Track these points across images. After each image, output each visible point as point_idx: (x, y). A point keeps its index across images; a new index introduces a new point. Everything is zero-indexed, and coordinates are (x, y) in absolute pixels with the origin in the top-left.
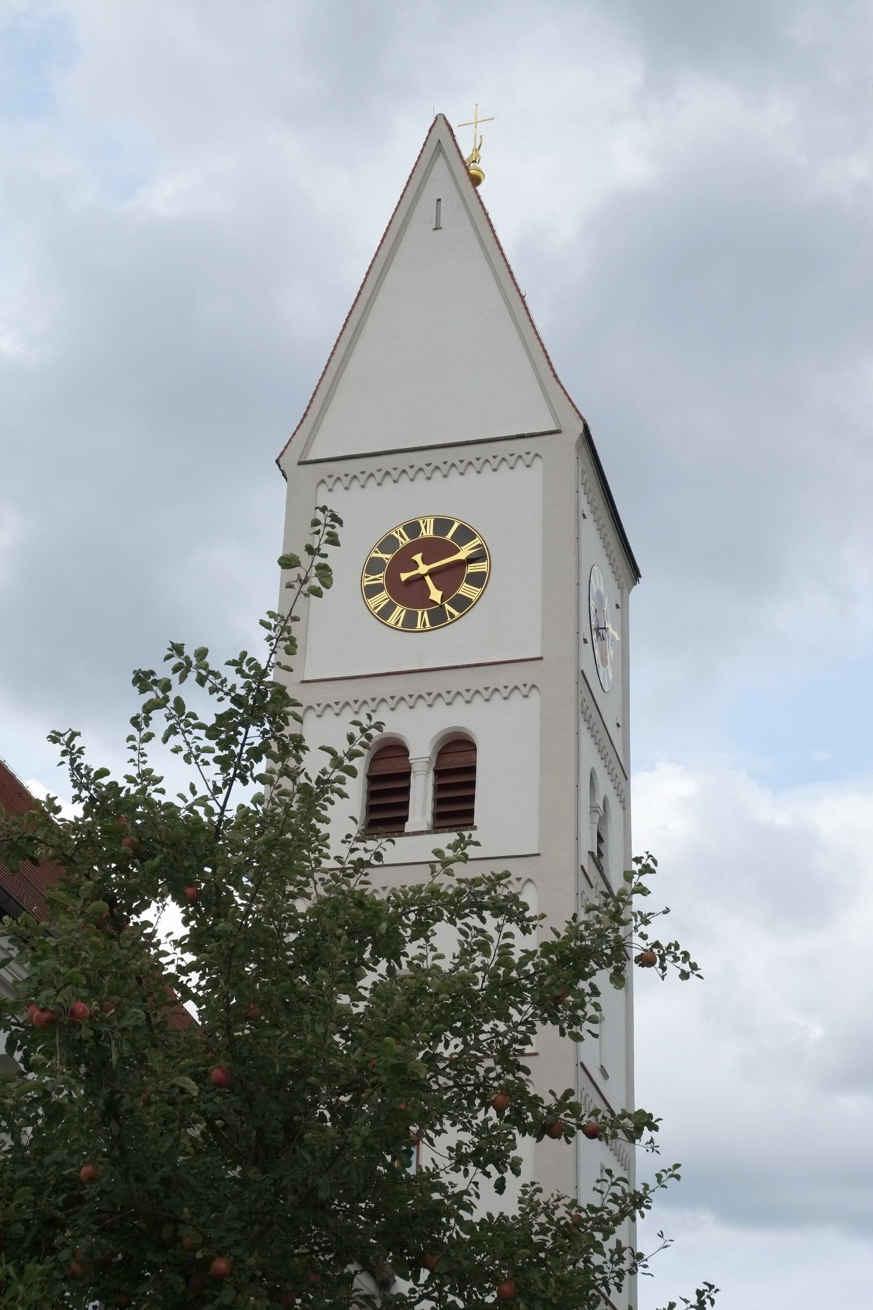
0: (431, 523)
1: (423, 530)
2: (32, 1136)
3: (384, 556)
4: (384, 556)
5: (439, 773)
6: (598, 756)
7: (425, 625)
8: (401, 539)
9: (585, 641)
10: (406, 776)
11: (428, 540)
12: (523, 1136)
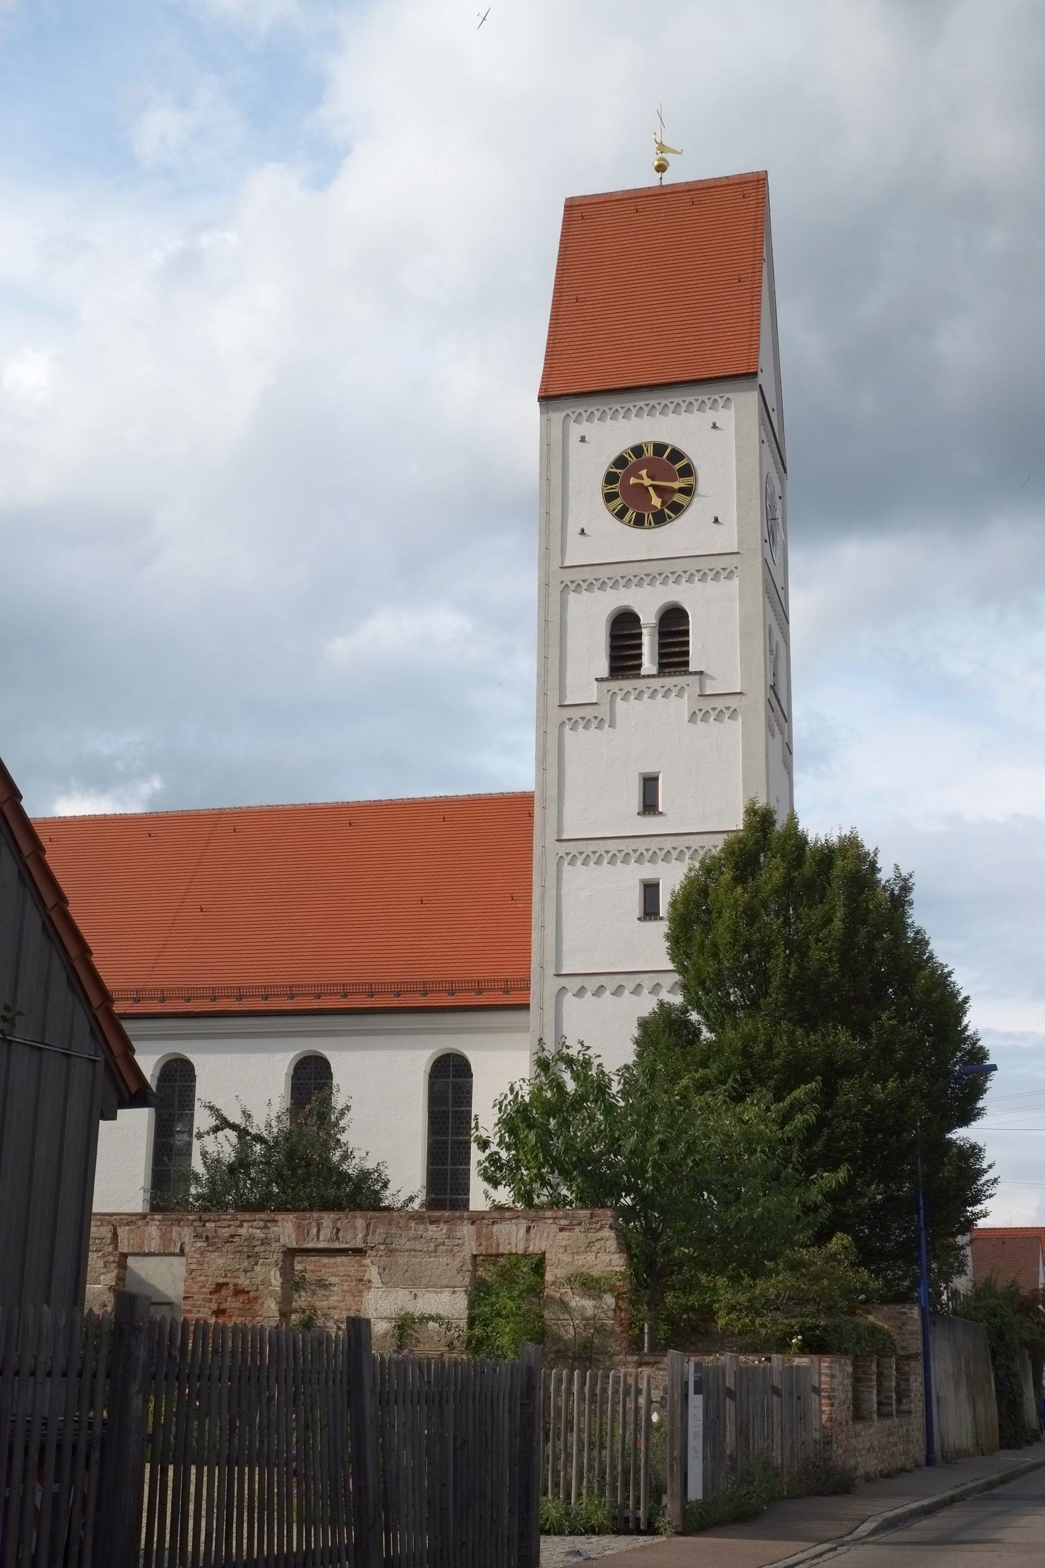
0: (651, 449)
1: (646, 452)
2: (802, 1086)
3: (618, 471)
4: (618, 471)
5: (662, 635)
6: (774, 618)
7: (650, 524)
8: (629, 458)
9: (766, 541)
10: (639, 636)
11: (649, 459)
12: (994, 1068)
